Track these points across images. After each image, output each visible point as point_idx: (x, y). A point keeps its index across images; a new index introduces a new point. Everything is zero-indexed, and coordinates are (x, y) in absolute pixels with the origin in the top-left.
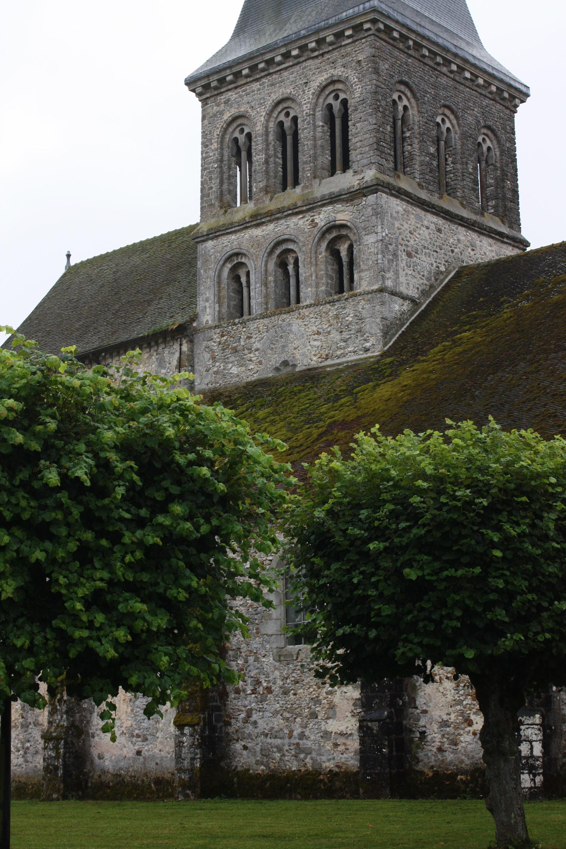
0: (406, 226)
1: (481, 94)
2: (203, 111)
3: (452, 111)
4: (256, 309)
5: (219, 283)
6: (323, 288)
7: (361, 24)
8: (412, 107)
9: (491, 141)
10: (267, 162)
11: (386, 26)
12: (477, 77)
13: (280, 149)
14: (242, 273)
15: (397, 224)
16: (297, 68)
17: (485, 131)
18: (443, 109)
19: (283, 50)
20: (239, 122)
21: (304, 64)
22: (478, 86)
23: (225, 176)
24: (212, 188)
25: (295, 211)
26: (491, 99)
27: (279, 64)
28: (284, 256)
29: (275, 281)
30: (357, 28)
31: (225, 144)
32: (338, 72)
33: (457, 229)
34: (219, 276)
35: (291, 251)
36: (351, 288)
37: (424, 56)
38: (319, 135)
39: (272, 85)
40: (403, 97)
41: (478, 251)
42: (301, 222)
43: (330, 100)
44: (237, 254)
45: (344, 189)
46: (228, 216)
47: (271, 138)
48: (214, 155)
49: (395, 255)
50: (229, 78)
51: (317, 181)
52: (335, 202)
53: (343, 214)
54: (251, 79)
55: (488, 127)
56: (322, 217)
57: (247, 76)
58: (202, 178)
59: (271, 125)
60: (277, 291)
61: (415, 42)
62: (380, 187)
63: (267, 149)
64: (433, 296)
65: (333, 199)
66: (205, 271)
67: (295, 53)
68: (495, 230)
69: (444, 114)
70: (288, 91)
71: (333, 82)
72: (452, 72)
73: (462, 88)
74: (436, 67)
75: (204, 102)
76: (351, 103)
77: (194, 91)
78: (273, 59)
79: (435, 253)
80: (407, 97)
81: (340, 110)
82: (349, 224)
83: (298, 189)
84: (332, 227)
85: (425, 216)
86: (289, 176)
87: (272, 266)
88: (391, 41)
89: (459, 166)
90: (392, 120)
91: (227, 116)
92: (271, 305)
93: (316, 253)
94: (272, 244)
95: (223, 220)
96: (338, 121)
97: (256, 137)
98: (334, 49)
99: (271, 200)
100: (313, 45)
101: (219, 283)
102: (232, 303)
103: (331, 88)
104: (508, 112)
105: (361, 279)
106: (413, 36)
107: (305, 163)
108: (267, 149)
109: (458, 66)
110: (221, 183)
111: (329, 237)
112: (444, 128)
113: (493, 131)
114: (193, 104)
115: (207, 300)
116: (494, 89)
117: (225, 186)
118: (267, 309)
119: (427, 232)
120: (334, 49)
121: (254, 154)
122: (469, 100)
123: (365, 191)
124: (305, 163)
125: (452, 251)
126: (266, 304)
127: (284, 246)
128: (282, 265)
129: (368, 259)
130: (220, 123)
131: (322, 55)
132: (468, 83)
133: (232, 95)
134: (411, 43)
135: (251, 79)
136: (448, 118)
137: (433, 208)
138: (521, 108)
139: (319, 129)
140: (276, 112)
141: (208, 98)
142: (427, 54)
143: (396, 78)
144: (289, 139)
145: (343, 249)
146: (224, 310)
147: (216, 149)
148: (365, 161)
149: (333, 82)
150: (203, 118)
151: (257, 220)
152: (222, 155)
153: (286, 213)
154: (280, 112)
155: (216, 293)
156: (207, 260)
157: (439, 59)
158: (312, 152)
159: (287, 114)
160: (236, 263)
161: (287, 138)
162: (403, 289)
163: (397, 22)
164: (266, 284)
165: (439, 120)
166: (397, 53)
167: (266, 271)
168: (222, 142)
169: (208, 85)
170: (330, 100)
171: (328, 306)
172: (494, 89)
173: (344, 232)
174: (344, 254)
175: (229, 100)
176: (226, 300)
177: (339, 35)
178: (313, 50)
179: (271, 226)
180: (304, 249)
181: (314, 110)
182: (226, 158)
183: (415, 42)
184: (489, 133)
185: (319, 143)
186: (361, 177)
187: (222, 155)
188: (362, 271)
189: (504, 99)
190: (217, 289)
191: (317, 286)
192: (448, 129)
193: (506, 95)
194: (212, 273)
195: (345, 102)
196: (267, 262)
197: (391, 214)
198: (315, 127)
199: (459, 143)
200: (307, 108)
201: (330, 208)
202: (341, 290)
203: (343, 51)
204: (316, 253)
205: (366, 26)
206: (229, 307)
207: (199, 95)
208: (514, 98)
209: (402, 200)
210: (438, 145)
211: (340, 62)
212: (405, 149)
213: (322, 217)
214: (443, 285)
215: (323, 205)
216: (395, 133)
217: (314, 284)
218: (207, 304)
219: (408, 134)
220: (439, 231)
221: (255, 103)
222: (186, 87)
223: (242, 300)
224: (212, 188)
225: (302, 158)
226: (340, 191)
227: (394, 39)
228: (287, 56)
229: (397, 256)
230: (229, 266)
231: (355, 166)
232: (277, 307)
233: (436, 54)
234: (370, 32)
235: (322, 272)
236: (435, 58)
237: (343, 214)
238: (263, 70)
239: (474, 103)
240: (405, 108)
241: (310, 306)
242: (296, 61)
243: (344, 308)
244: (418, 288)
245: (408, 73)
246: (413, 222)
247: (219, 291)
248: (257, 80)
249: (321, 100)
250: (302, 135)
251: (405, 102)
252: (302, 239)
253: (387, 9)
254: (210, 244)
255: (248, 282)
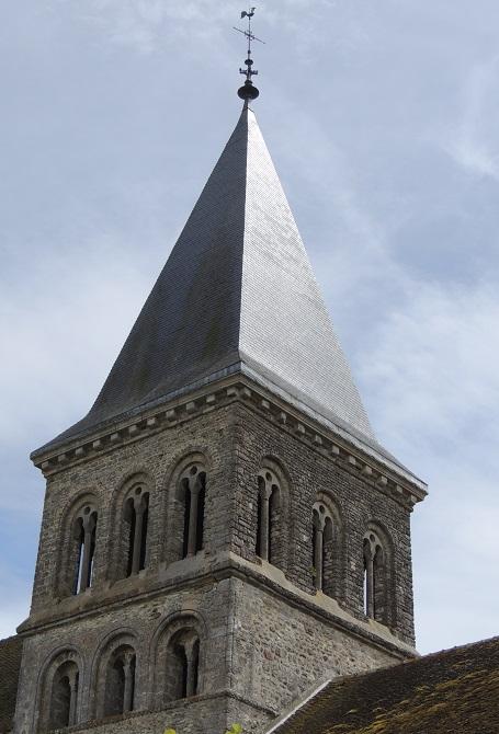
0: (266, 621)
1: (369, 484)
2: (48, 488)
3: (333, 500)
4: (82, 718)
5: (43, 686)
6: (161, 692)
7: (225, 390)
8: (283, 488)
9: (381, 539)
10: (110, 544)
11: (253, 393)
12: (364, 465)
13: (127, 531)
14: (71, 674)
15: (254, 617)
16: (153, 438)
17: (371, 526)
18: (321, 495)
19: (138, 420)
20: (84, 500)
21: (161, 435)
22: (367, 476)
23: (64, 561)
24: (47, 574)
25: (135, 599)
26: (381, 492)
27: (133, 435)
28: (121, 654)
29: (107, 684)
30: (220, 394)
31: (68, 526)
32: (198, 442)
33: (333, 632)
34: (44, 678)
35: (129, 647)
36: (195, 693)
37: (299, 433)
38: (170, 513)
39: (125, 458)
40: (272, 474)
41: (358, 662)
42: (141, 613)
43: (186, 474)
44: (67, 651)
45: (193, 573)
46: (61, 606)
47: (118, 516)
48: (53, 537)
49: (249, 654)
50: (78, 451)
51: (164, 564)
52: (182, 588)
53: (189, 602)
54: (102, 452)
55: (378, 523)
56: (165, 606)
57: (98, 449)
58: (38, 562)
59: (120, 502)
60: (109, 696)
61: (289, 416)
62: (234, 571)
63: (112, 530)
64: (296, 709)
65: (180, 585)
66: (28, 671)
67: (151, 422)
68: (381, 640)
69: (321, 501)
70: (141, 464)
71: (191, 454)
72: (333, 455)
73: (346, 475)
74: (314, 447)
75: (50, 479)
76: (209, 476)
77: (39, 466)
78: (127, 429)
79: (301, 658)
80: (277, 477)
81: (197, 485)
82: (196, 614)
83: (142, 575)
84: (177, 618)
85: (292, 611)
86: (135, 560)
87: (104, 666)
88: (260, 411)
89: (338, 562)
90: (256, 498)
91: (72, 494)
92: (100, 711)
93: (156, 649)
94: (107, 639)
95: (55, 610)
96: (193, 499)
97: (101, 516)
98: (194, 418)
99: (110, 587)
100: (172, 412)
101: (43, 686)
102: (56, 711)
103: (188, 461)
104: (401, 509)
105: (205, 680)
106: (287, 410)
107: (153, 544)
108: (112, 530)
109: (341, 450)
110: (58, 570)
111: (173, 630)
112: (322, 518)
113: (383, 528)
114: (38, 481)
115: (27, 706)
116: (384, 481)
117: (63, 573)
118: (94, 717)
119: (293, 631)
120: (194, 418)
121: (97, 535)
122: (354, 489)
123: (215, 575)
124: (153, 544)
125: (326, 659)
126: (94, 712)
127: (121, 642)
128: (118, 664)
129: (215, 656)
130: (64, 502)
131: (181, 424)
132: (353, 471)
133: (81, 471)
134: (284, 416)
135: (102, 452)
136: (328, 506)
137: (301, 603)
138: (417, 507)
139: (172, 506)
140: (127, 489)
141: (53, 475)
142: (303, 431)
143: (264, 453)
144: (139, 518)
145: (189, 645)
146: (45, 719)
147: (57, 531)
148: (219, 541)
149: (191, 454)
150: (47, 496)
151: (91, 610)
152: (63, 537)
153: (125, 602)
154: (130, 489)
155: (38, 697)
156: (32, 658)
157: (317, 438)
158: (160, 532)
159: (139, 491)
160: (64, 660)
161: (136, 518)
162: (256, 698)
163: (268, 391)
164: (95, 688)
165: (316, 506)
166: (266, 425)
167: (98, 671)
168: (64, 523)
169: (54, 459)
170: (186, 474)
171: (164, 714)
172: (384, 481)
173: (190, 625)
174: (189, 652)
175: (76, 476)
176: (48, 707)
177: (200, 403)
178: (171, 419)
179: (108, 618)
180: (142, 644)
181: (168, 484)
182: (67, 540)
183: (289, 416)
184: (379, 530)
185: (170, 522)
186: (213, 559)
187: (63, 537)
188: (206, 671)
189: (397, 494)
190: (39, 692)
191: (154, 689)
192: (327, 519)
193: (399, 490)
194: (35, 673)
195: (202, 477)
196: (99, 660)
197: (247, 604)
198: (167, 504)
199: (339, 536)
200: (159, 483)
201: (175, 595)
202: (184, 695)
203: (204, 420)
204: (156, 649)
205: (230, 392)
206: (51, 715)
207: (44, 471)
208: (410, 494)
209: (263, 589)
210: (314, 534)
211: (200, 432)
212: (273, 535)
213: (165, 606)
214: (311, 697)
215: (168, 592)
216: (260, 512)
217: (150, 686)
218: (26, 712)
219: (277, 518)
220: (309, 632)
221: (104, 479)
222: (32, 462)
223: (68, 709)
224: (47, 574)
225: (150, 539)
226: (188, 575)
227: (263, 409)
228: (142, 426)
229: (251, 656)
230: (57, 665)
231: (207, 547)
232: (106, 715)
233: (315, 433)
234: (234, 399)
235: (162, 673)
236: (314, 437)
237: (189, 602)
238: (116, 442)
239: (361, 494)
240: (274, 488)
241: (142, 714)
242: (151, 432)
243: (183, 716)
244: (277, 699)
245: (278, 449)
246: (275, 619)
247: (42, 695)
248: (109, 453)
249: (176, 474)
250: (152, 512)
251: (275, 481)
252: (140, 632)
253: (256, 375)
254: (38, 638)
255: (77, 685)
